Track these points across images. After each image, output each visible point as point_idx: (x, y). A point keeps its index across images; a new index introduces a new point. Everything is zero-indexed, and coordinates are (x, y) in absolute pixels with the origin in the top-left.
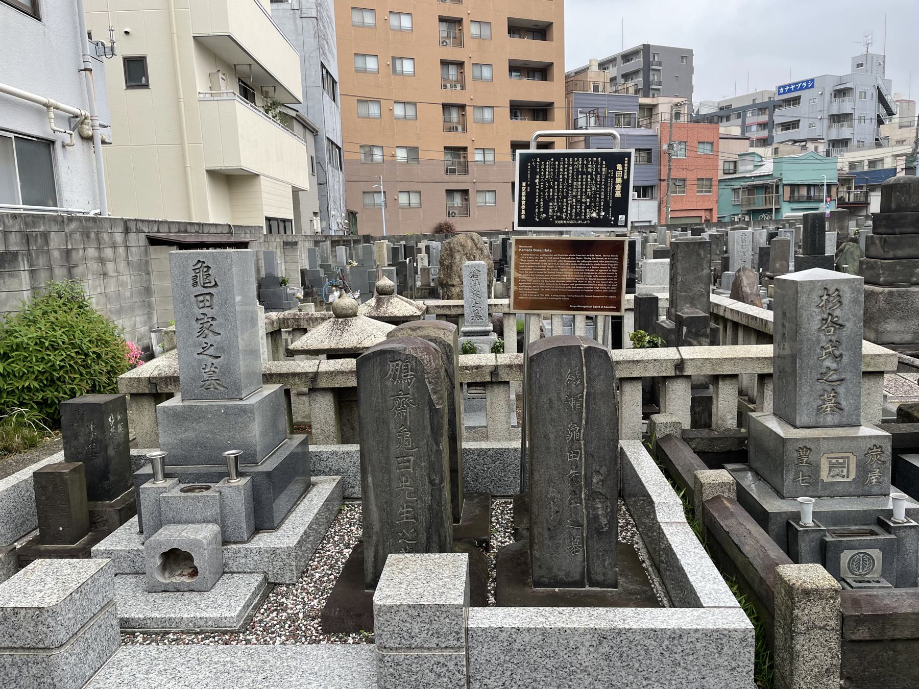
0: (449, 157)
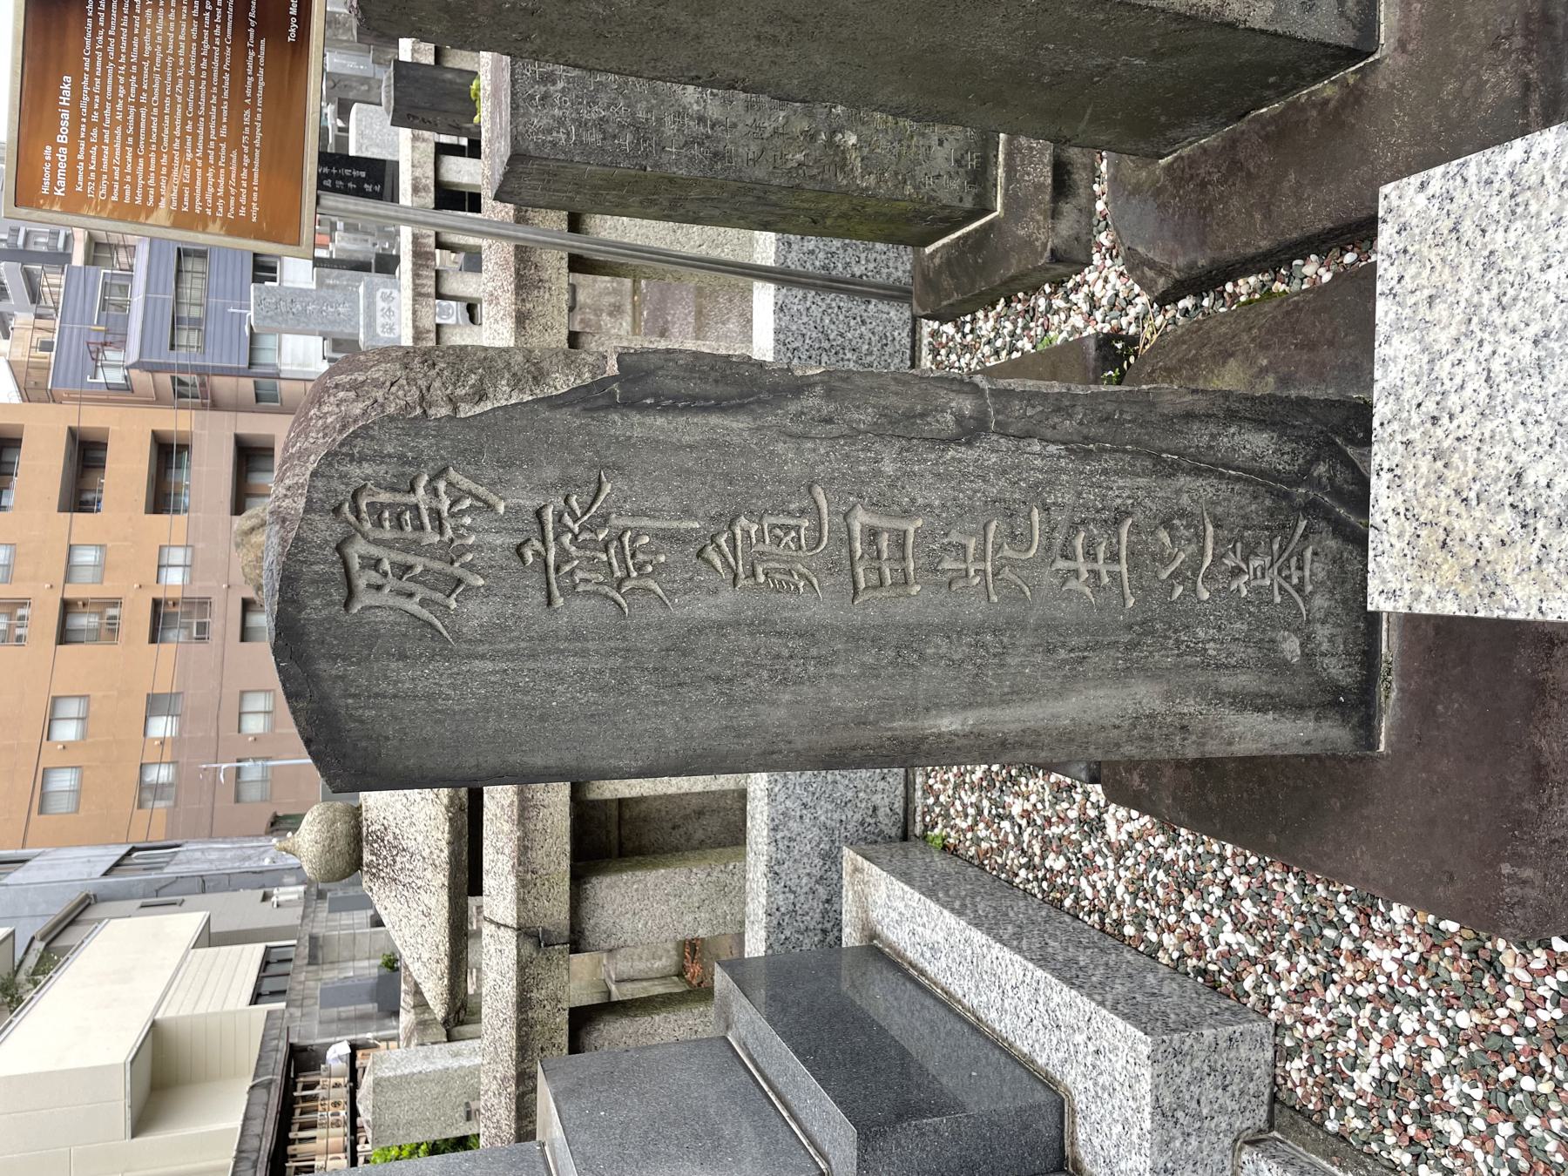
0: (171, 635)
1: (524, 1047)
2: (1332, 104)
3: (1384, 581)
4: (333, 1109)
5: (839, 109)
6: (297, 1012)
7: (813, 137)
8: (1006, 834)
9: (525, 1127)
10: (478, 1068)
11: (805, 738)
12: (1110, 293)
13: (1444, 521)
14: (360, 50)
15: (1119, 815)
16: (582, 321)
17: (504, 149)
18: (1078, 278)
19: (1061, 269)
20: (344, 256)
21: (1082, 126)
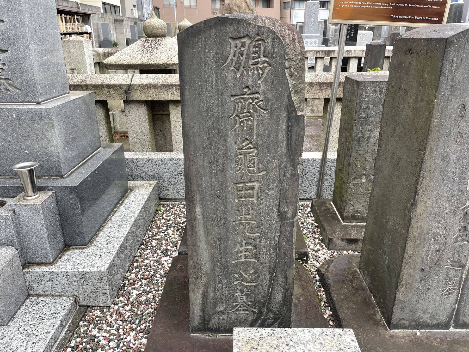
1: (96, 87)
2: (374, 317)
3: (242, 332)
4: (71, 27)
5: (372, 177)
6: (100, 16)
7: (364, 169)
8: (162, 228)
9: (75, 87)
10: (87, 73)
11: (194, 170)
12: (320, 256)
13: (259, 348)
14: (389, 33)
15: (169, 261)
16: (309, 101)
17: (361, 79)
18: (324, 246)
19: (327, 241)
20: (328, 29)
21: (368, 246)
